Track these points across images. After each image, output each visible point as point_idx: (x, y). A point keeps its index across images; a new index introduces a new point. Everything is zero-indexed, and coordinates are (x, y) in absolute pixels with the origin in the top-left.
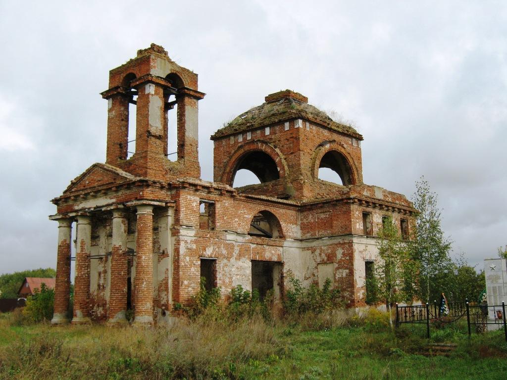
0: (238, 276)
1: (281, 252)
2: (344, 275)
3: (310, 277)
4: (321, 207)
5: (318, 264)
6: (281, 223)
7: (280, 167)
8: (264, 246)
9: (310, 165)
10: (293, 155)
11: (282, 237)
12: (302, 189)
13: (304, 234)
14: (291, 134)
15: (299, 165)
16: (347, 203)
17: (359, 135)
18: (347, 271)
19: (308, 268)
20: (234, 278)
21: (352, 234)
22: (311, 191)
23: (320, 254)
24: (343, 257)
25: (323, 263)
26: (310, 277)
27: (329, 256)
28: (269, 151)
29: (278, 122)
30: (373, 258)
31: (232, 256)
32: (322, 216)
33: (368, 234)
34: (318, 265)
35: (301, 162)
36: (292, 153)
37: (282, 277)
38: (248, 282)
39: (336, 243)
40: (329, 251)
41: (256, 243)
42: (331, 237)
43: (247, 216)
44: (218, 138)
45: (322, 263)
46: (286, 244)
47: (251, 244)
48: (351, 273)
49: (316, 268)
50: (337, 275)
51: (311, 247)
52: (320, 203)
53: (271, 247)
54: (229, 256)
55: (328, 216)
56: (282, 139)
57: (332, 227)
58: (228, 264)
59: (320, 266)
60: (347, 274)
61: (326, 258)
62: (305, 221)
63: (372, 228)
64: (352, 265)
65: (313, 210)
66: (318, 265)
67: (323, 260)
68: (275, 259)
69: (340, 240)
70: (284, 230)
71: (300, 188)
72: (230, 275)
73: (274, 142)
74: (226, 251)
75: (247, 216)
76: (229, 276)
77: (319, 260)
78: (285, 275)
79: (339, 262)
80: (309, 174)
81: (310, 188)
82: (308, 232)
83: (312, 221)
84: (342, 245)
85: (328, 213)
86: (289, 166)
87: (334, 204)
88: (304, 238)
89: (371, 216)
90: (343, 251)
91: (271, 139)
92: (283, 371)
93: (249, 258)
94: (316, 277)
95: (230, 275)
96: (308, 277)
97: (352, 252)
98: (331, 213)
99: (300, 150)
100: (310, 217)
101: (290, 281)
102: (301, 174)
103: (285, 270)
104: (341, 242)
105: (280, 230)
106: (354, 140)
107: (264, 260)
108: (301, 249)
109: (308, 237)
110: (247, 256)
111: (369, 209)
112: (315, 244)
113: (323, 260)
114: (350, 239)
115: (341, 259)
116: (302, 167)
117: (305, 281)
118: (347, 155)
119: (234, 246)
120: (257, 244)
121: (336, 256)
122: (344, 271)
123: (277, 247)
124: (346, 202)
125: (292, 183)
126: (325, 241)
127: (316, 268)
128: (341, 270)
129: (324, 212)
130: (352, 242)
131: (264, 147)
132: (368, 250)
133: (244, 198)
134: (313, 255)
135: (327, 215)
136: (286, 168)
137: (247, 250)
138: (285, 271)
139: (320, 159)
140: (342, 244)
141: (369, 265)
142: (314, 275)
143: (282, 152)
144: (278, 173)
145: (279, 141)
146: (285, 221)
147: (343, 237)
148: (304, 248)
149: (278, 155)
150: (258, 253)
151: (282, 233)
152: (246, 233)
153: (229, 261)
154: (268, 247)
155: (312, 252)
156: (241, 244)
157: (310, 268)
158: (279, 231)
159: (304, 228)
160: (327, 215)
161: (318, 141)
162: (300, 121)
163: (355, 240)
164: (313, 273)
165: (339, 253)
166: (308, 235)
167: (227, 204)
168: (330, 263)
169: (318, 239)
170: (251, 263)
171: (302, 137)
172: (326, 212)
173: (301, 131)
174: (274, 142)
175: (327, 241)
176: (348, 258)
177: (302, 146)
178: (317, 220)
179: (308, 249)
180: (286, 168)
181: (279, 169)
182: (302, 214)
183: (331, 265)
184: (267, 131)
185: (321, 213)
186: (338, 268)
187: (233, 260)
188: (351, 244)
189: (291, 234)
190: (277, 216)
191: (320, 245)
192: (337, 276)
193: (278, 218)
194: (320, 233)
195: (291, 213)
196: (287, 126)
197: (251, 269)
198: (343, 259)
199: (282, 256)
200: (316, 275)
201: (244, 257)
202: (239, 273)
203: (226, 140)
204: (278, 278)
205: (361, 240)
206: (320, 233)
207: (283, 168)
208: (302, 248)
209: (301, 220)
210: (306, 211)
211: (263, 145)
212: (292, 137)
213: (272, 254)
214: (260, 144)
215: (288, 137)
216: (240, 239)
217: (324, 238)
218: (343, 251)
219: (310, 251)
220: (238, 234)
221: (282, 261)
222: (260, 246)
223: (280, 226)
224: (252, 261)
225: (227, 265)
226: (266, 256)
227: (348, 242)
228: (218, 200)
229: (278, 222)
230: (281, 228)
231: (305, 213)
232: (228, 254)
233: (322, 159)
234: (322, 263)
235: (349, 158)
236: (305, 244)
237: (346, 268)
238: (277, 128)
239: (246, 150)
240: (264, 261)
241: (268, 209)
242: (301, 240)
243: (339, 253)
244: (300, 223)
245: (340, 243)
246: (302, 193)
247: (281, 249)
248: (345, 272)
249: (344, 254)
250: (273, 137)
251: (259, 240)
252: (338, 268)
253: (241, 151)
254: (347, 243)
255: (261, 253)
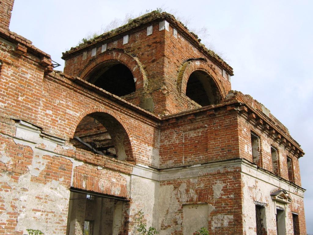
0: (38, 214)
1: (128, 183)
2: (226, 223)
3: (169, 226)
4: (191, 121)
5: (184, 205)
6: (131, 139)
7: (137, 77)
8: (99, 168)
9: (177, 78)
10: (155, 63)
11: (131, 159)
12: (165, 100)
13: (164, 161)
14: (154, 38)
15: (163, 73)
16: (233, 112)
17: (230, 67)
18: (232, 217)
19: (168, 211)
20: (22, 215)
21: (239, 159)
22: (176, 106)
23: (187, 191)
24: (225, 195)
25: (192, 203)
26: (169, 226)
27: (200, 193)
28: (125, 59)
29: (139, 27)
30: (264, 201)
31: (24, 170)
32: (192, 134)
33: (257, 163)
34: (182, 208)
35: (165, 70)
36: (153, 61)
37: (126, 223)
38: (59, 227)
39: (213, 172)
40: (202, 185)
41: (83, 159)
42: (205, 163)
43: (71, 112)
44: (66, 56)
45: (190, 204)
46: (136, 170)
47: (73, 160)
48: (238, 221)
49: (180, 211)
50: (213, 223)
51: (174, 180)
52: (190, 115)
53: (111, 171)
54: (18, 170)
55: (200, 134)
56: (143, 46)
57: (206, 149)
58: (13, 184)
59: (186, 210)
60: (230, 222)
61: (195, 197)
62: (166, 143)
63: (261, 158)
64: (240, 207)
65: (178, 126)
66: (182, 208)
67: (192, 200)
68: (116, 192)
69: (219, 168)
70: (135, 149)
71: (162, 100)
72: (14, 207)
73: (132, 51)
74: (10, 158)
75: (71, 112)
76: (10, 210)
77: (184, 199)
78: (130, 219)
79: (217, 202)
80: (175, 87)
81: (175, 103)
82: (170, 159)
83: (177, 142)
84: (220, 175)
85: (201, 130)
86: (148, 76)
87: (210, 115)
88: (164, 166)
89: (259, 141)
90: (224, 185)
91: (129, 48)
92: (166, 221)
93: (67, 183)
94: (180, 226)
95: (14, 207)
96: (166, 225)
97: (240, 186)
98: (206, 129)
99: (164, 56)
100: (175, 136)
101: (139, 230)
102: (164, 84)
103: (133, 211)
104: (222, 171)
105: (129, 151)
106: (224, 72)
107: (96, 191)
108: (158, 184)
109: (171, 166)
110: (62, 179)
111: (258, 131)
112: (178, 175)
113: (192, 200)
114: (236, 166)
115: (221, 198)
116: (166, 76)
117: (163, 231)
118: (219, 82)
119: (31, 151)
120: (86, 162)
121: (212, 193)
122: (226, 217)
123: (121, 174)
124: (230, 111)
125: (151, 94)
126: (195, 171)
127: (180, 211)
128: (220, 216)
129: (194, 129)
130: (240, 171)
131: (119, 56)
132: (258, 188)
133: (70, 83)
134: (175, 192)
135: (200, 132)
136: (145, 78)
137: (65, 169)
138: (131, 213)
139: (190, 74)
140: (224, 174)
141: (260, 209)
142: (176, 223)
143: (140, 61)
144: (134, 84)
145: (139, 48)
146: (137, 138)
147: (224, 164)
148: (164, 181)
149: (136, 63)
150: (86, 178)
151: (132, 154)
152: (67, 138)
153: (16, 179)
154: (105, 171)
155: (175, 188)
156: (52, 155)
157: (170, 211)
158: (126, 151)
159: (163, 152)
160: (200, 132)
161: (187, 56)
162: (167, 24)
163: (245, 168)
164: (176, 219)
165: (218, 189)
166: (170, 163)
167: (29, 76)
168: (202, 204)
169: (184, 167)
170: (69, 192)
171: (167, 42)
172: (198, 128)
173: (167, 35)
174: (132, 51)
175: (198, 170)
176: (232, 196)
177: (167, 52)
178: (183, 141)
179: (169, 183)
180: (145, 78)
181: (135, 80)
182: (163, 133)
183: (204, 208)
184: (126, 40)
185: (190, 130)
186: (215, 213)
187: (24, 179)
188: (237, 174)
189: (145, 159)
190: (125, 126)
191: (188, 177)
192: (214, 225)
193: (127, 131)
194: (188, 159)
195: (148, 129)
196: (150, 30)
197: (68, 202)
198: (224, 197)
199: (128, 188)
200: (179, 222)
201: (56, 180)
202: (40, 207)
203: (77, 57)
204: (120, 225)
205: (251, 170)
206: (188, 159)
207: (141, 79)
208: (160, 182)
209: (162, 141)
210: (168, 128)
211: (119, 54)
212: (156, 43)
213: (112, 183)
214: (114, 54)
215: (150, 43)
216: (50, 145)
217: (195, 166)
218: (224, 185)
219: (172, 186)
220: (44, 135)
221: (128, 198)
222: (90, 167)
223: (129, 143)
224: (72, 189)
225: (10, 187)
226: (100, 184)
227: (233, 170)
228: (10, 61)
229: (127, 137)
230: (131, 147)
231: (168, 132)
232: (15, 165)
233: (190, 75)
234: (190, 204)
235: (220, 85)
236: (164, 176)
237: (230, 213)
238: (138, 35)
239: (98, 63)
240: (97, 193)
241: (110, 112)
242: (159, 170)
243: (218, 189)
244: (158, 146)
245: (219, 173)
246: (164, 106)
247: (127, 178)
248: (227, 220)
249: (225, 190)
250: (132, 45)
251: (89, 156)
252: (215, 213)
253: (93, 65)
254: (231, 172)
255: (92, 179)
